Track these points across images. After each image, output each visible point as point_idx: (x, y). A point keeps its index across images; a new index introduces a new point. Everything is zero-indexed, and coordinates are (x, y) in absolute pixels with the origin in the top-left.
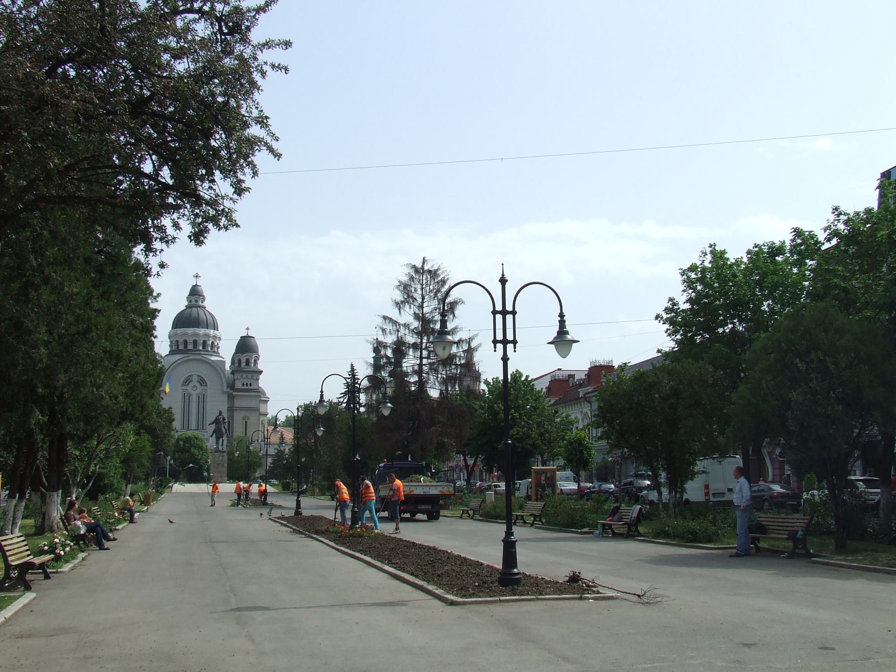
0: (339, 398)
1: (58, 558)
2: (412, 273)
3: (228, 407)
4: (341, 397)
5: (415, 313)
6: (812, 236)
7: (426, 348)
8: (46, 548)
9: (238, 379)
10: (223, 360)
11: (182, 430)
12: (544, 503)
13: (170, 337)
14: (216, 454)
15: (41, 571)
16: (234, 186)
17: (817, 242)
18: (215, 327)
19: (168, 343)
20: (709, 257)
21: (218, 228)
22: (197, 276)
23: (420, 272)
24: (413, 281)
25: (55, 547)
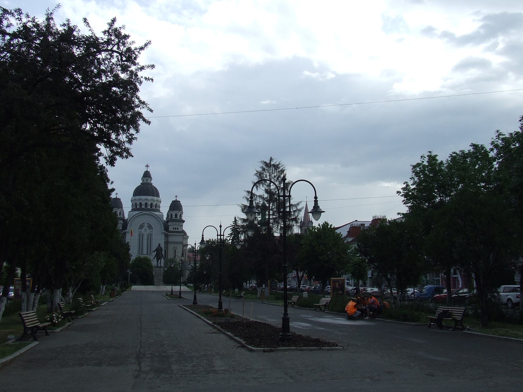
0: (228, 237)
1: (54, 325)
2: (264, 167)
3: (165, 242)
4: (229, 236)
5: (266, 189)
6: (483, 147)
7: (272, 210)
8: (48, 319)
9: (171, 225)
10: (162, 214)
11: (138, 255)
12: (298, 296)
13: (132, 201)
14: (157, 269)
15: (44, 331)
16: (127, 137)
17: (486, 152)
18: (158, 195)
19: (130, 204)
20: (427, 159)
21: (122, 158)
22: (147, 166)
23: (269, 166)
24: (265, 171)
25: (53, 319)
